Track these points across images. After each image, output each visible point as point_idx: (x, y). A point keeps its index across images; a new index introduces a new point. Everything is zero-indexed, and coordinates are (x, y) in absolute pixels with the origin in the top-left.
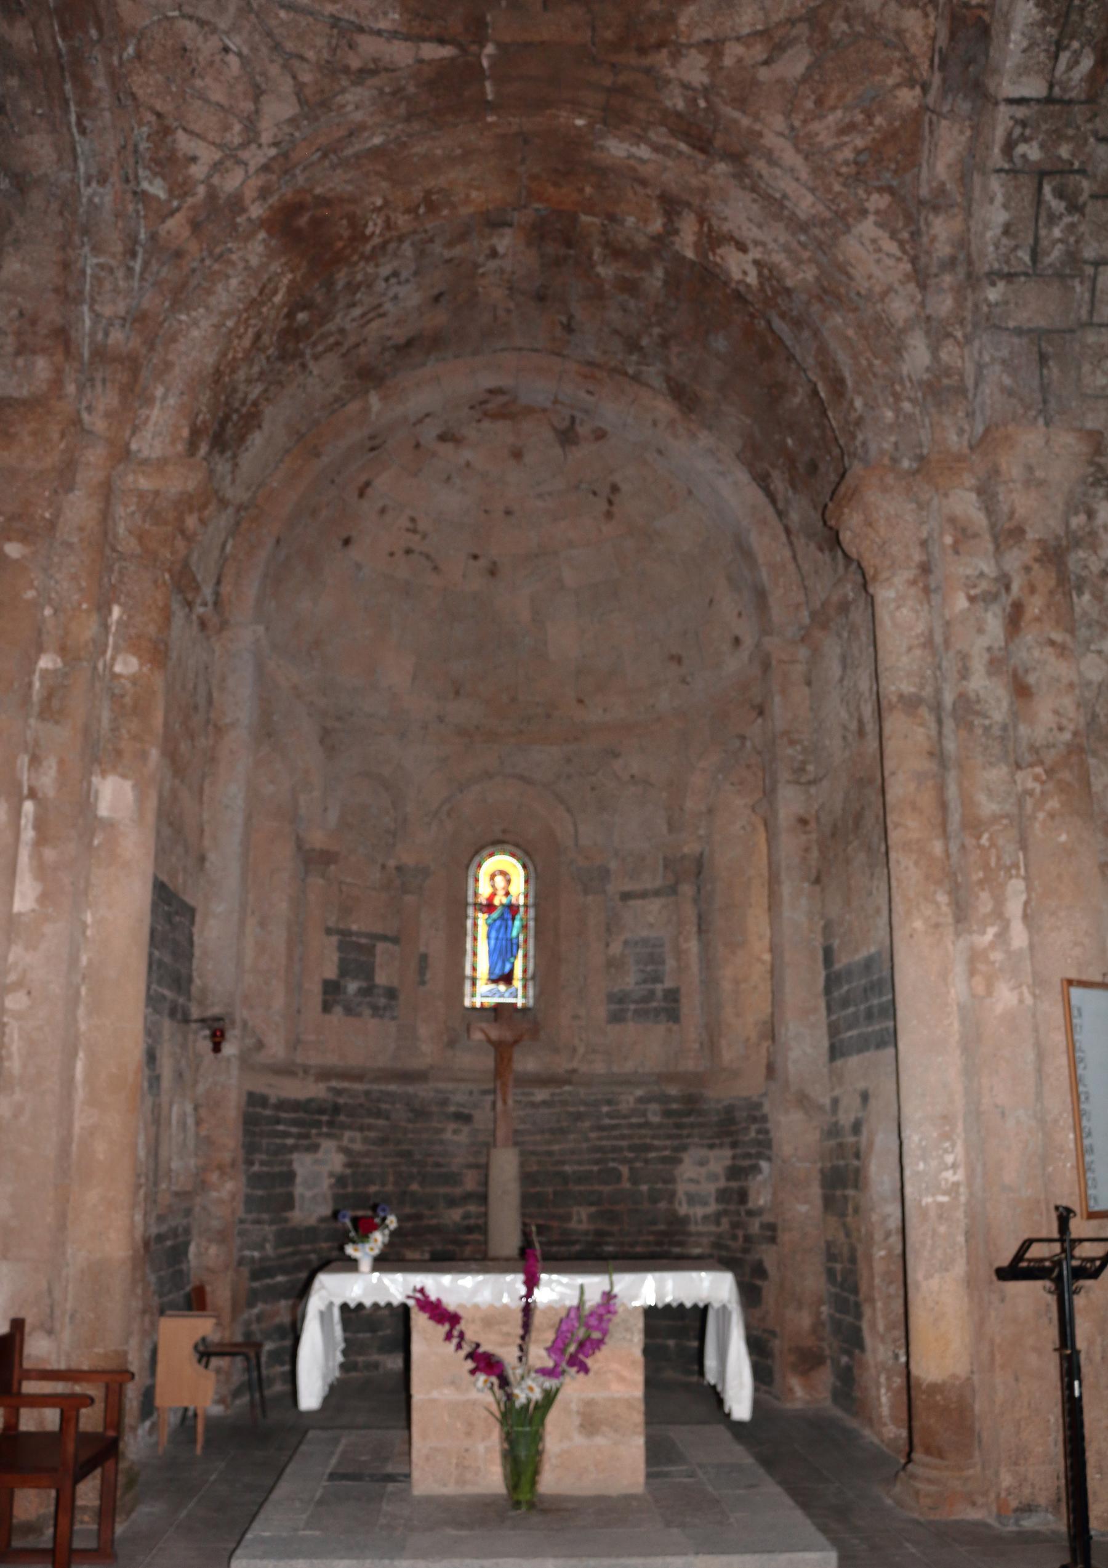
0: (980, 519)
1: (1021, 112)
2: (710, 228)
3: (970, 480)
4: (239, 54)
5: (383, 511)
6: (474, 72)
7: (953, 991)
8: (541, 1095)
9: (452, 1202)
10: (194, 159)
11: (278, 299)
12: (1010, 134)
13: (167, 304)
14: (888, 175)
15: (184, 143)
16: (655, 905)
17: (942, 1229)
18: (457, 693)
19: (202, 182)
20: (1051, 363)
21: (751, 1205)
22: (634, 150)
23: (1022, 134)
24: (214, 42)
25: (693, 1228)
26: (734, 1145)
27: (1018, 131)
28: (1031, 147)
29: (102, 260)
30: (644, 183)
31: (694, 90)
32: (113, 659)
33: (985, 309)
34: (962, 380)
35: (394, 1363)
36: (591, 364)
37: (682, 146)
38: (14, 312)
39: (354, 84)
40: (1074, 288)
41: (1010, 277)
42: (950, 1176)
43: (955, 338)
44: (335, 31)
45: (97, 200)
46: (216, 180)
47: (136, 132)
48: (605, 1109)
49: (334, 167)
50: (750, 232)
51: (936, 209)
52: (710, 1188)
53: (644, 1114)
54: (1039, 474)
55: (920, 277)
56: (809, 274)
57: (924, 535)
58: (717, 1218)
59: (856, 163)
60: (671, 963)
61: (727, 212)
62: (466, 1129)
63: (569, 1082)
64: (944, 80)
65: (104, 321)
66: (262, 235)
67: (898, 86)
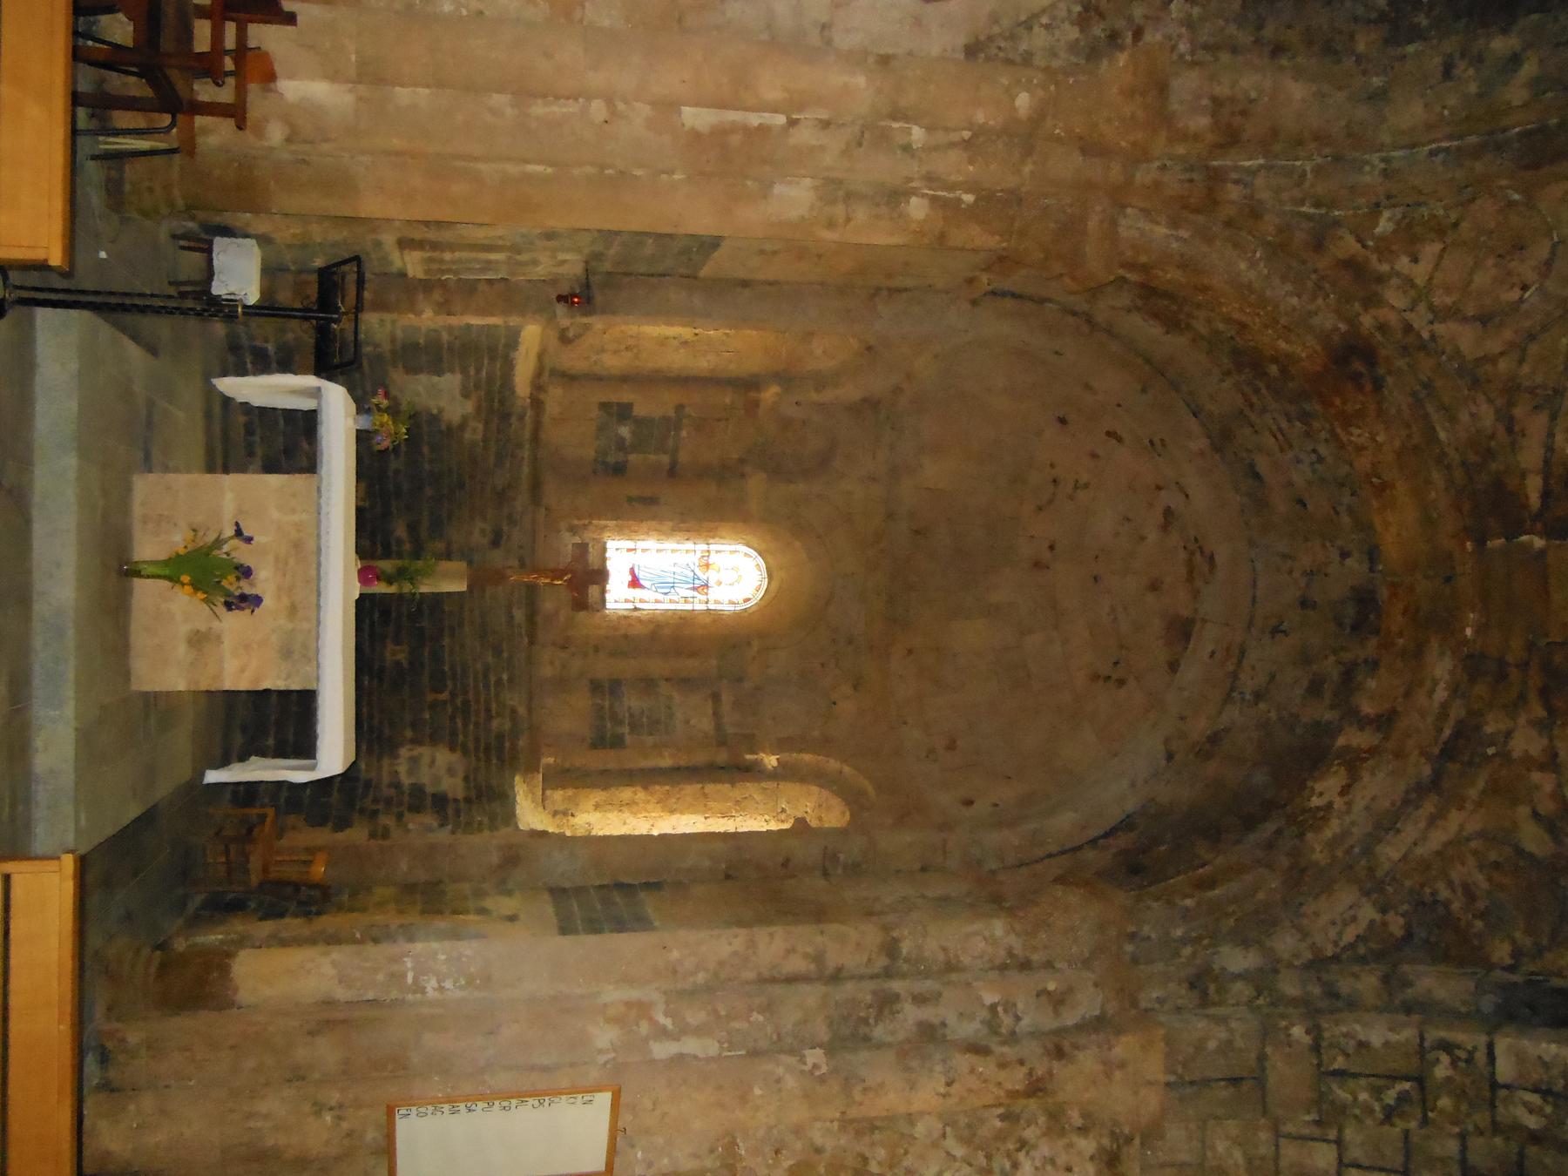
0: (1070, 1018)
1: (1481, 1057)
2: (1365, 760)
3: (1112, 1008)
4: (1521, 300)
5: (1094, 456)
6: (1513, 529)
7: (611, 987)
8: (519, 615)
9: (413, 528)
10: (1415, 260)
11: (1282, 345)
12: (1459, 1047)
13: (1270, 238)
14: (1423, 935)
15: (1431, 250)
16: (705, 724)
17: (380, 977)
18: (917, 532)
19: (1392, 268)
20: (1232, 1090)
21: (408, 816)
22: (1442, 685)
23: (1459, 1059)
24: (1531, 276)
25: (386, 762)
26: (468, 800)
27: (1462, 1054)
28: (1447, 1069)
29: (1309, 175)
30: (1407, 695)
31: (1506, 743)
32: (923, 195)
33: (1284, 1023)
34: (1214, 1004)
35: (274, 698)
36: (1242, 653)
37: (1447, 732)
38: (1253, 95)
39: (1497, 411)
40: (1309, 1113)
41: (1316, 1048)
42: (431, 984)
43: (1257, 998)
44: (1550, 392)
45: (1367, 168)
46: (1395, 281)
47: (1439, 203)
48: (505, 677)
49: (1414, 394)
50: (1361, 797)
51: (1386, 979)
52: (424, 777)
53: (498, 714)
54: (1118, 1075)
55: (1318, 964)
56: (1319, 856)
57: (1058, 965)
58: (397, 785)
59: (1436, 902)
60: (650, 740)
61: (1381, 775)
62: (485, 541)
63: (532, 643)
64: (1515, 984)
65: (1249, 179)
66: (1343, 327)
67: (1513, 942)
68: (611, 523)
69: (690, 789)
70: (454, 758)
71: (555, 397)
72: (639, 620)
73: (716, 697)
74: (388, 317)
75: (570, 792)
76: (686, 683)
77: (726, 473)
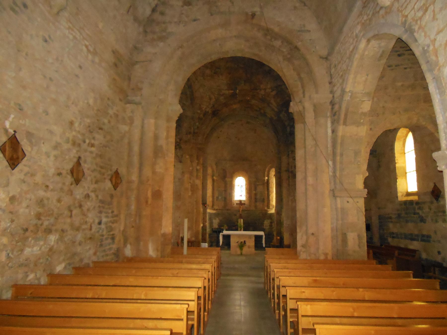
68: (233, 199)
69: (270, 189)
71: (216, 207)
72: (246, 195)
73: (258, 185)
75: (270, 206)
76: (255, 189)
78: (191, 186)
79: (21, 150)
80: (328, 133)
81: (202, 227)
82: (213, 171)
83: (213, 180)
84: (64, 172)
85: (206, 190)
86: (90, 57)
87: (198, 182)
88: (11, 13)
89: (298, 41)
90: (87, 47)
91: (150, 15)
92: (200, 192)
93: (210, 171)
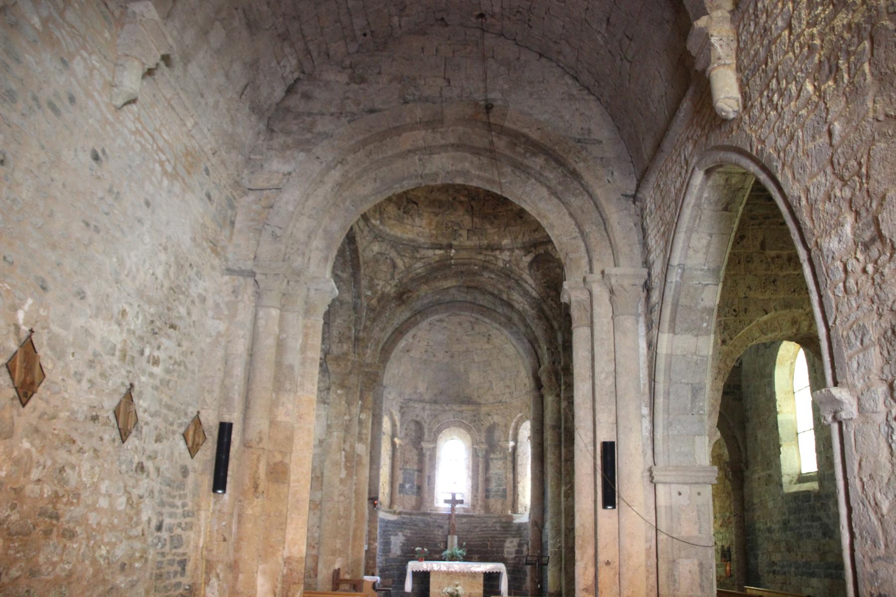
8: (465, 520)
16: (500, 463)
26: (520, 537)
52: (513, 550)
58: (516, 558)
62: (441, 530)
70: (508, 541)
71: (397, 508)
74: (377, 556)
75: (519, 506)
77: (421, 455)
78: (346, 457)
79: (37, 367)
80: (641, 349)
81: (366, 551)
82: (394, 425)
83: (393, 444)
84: (103, 414)
85: (378, 468)
86: (166, 182)
87: (362, 449)
88: (49, 112)
89: (578, 160)
90: (162, 163)
91: (283, 100)
92: (365, 472)
93: (386, 425)
